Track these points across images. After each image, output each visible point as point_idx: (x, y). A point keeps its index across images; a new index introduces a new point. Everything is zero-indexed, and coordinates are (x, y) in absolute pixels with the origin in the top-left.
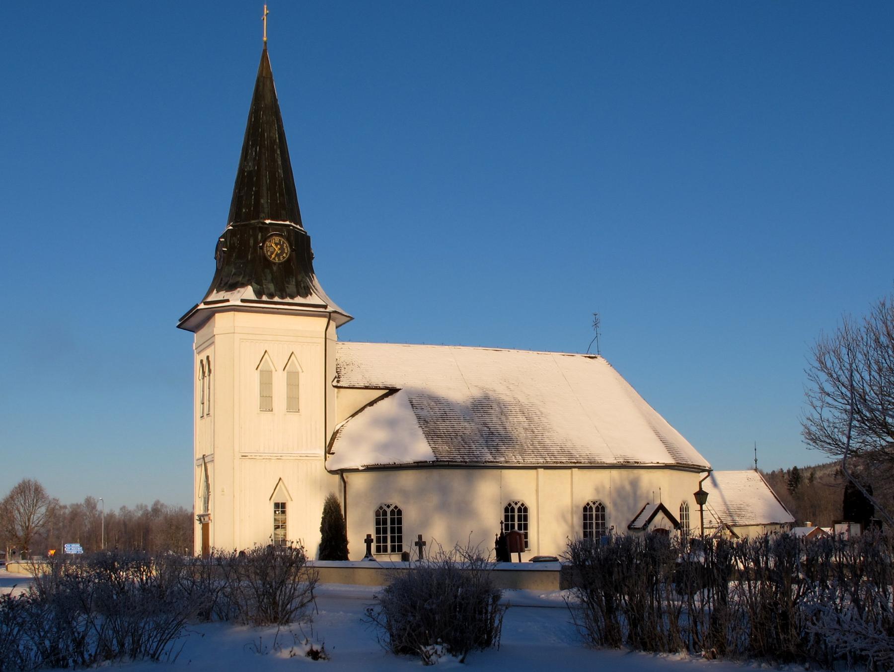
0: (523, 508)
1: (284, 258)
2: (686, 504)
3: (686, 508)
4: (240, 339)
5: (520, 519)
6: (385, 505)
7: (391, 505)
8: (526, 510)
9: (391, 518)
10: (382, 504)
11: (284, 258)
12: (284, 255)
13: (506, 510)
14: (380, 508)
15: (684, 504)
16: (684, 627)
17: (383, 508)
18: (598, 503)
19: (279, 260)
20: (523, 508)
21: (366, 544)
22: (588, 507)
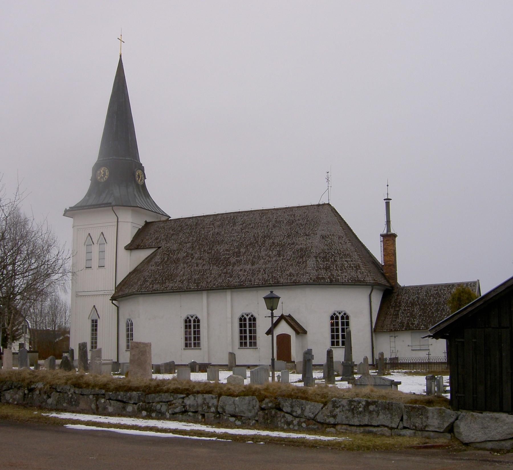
0: (196, 320)
1: (106, 178)
2: (130, 321)
3: (130, 324)
4: (78, 229)
5: (245, 331)
6: (338, 312)
7: (342, 312)
8: (199, 321)
9: (246, 328)
10: (243, 313)
11: (106, 178)
12: (106, 177)
13: (186, 321)
14: (333, 314)
15: (130, 321)
16: (53, 385)
17: (336, 314)
18: (343, 313)
19: (103, 180)
20: (196, 320)
21: (353, 361)
22: (243, 318)
